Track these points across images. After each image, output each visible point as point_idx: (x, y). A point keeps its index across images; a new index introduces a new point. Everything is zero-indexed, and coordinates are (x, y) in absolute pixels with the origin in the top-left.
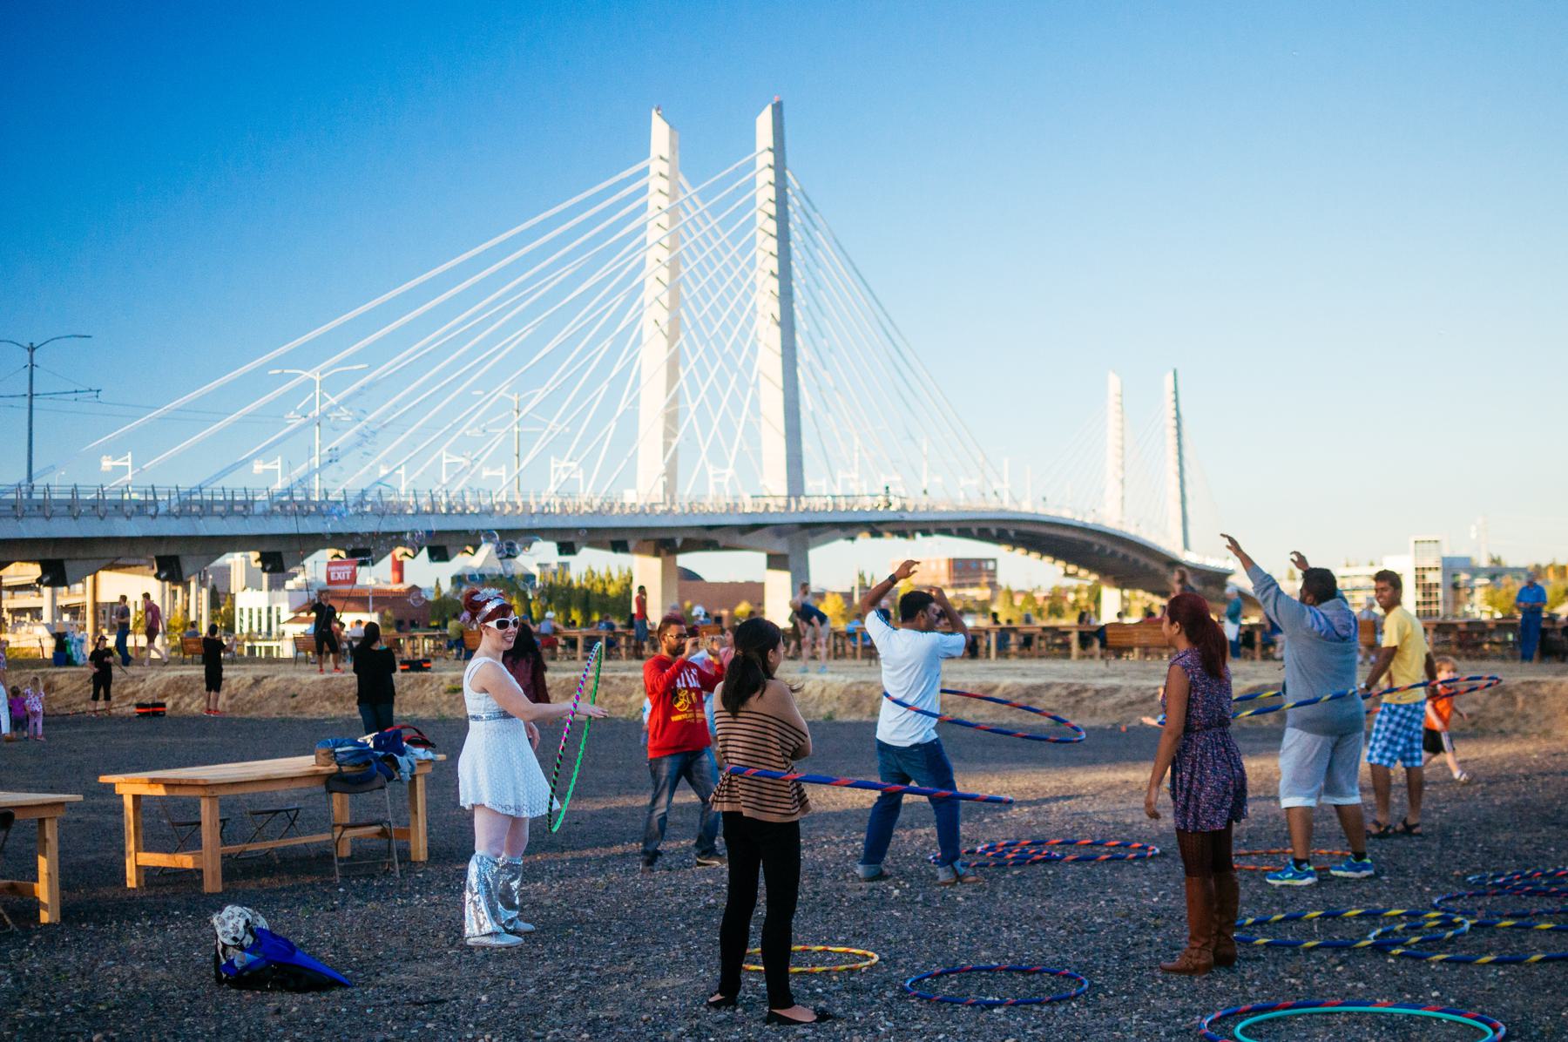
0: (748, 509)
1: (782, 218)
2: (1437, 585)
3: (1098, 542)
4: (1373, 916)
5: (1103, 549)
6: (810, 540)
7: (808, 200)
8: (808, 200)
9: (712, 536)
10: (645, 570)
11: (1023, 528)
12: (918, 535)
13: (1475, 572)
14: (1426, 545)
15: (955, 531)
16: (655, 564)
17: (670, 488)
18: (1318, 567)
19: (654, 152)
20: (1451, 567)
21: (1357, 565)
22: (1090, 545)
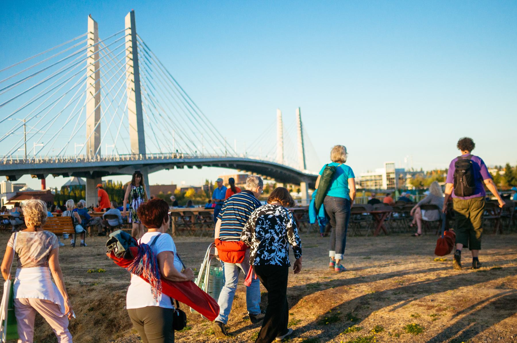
0: (118, 160)
1: (135, 53)
2: (394, 178)
3: (270, 168)
5: (277, 171)
6: (149, 170)
7: (146, 46)
8: (146, 46)
11: (239, 163)
12: (186, 167)
13: (405, 173)
14: (390, 165)
15: (220, 165)
18: (160, 184)
19: (89, 31)
20: (398, 172)
21: (371, 172)
22: (267, 169)
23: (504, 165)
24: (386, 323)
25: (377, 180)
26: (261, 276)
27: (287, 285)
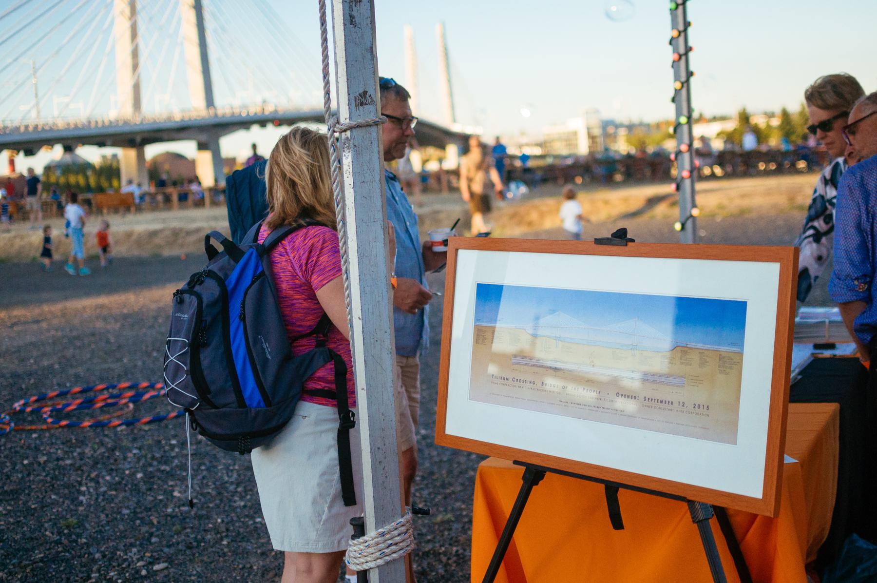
4: (152, 387)
9: (159, 135)
10: (125, 156)
13: (617, 126)
16: (132, 153)
17: (137, 103)
20: (605, 125)
23: (778, 110)
24: (43, 499)
25: (570, 139)
26: (313, 390)
27: (783, 461)
